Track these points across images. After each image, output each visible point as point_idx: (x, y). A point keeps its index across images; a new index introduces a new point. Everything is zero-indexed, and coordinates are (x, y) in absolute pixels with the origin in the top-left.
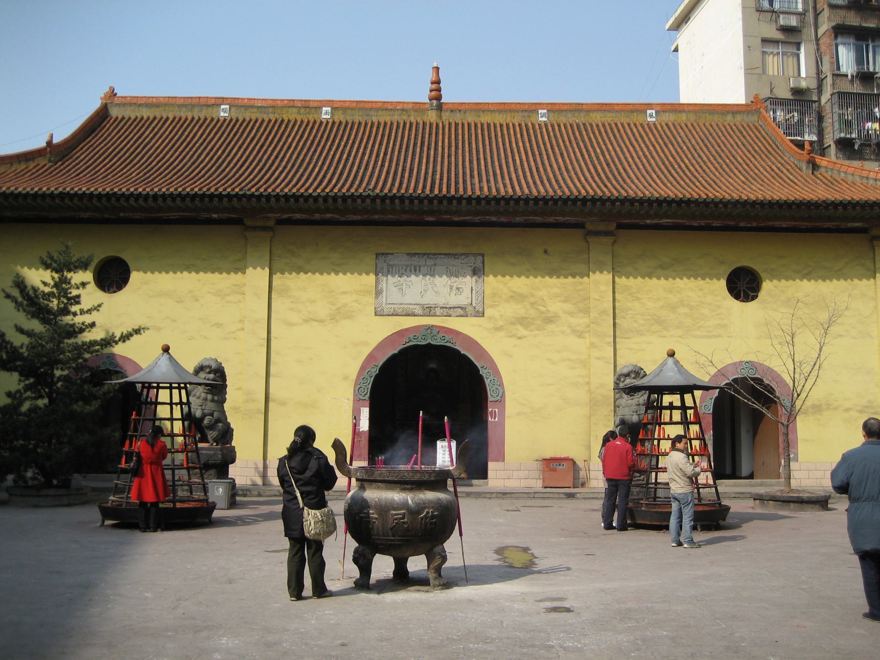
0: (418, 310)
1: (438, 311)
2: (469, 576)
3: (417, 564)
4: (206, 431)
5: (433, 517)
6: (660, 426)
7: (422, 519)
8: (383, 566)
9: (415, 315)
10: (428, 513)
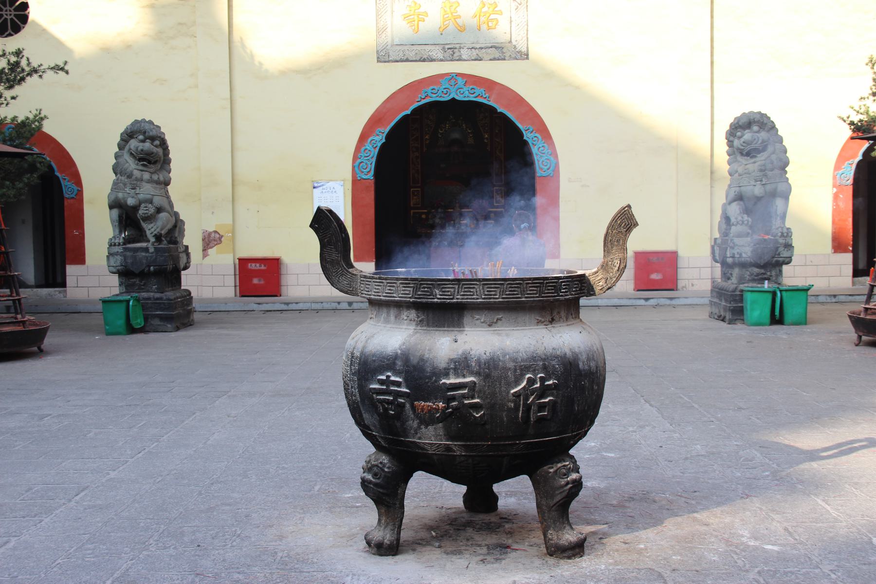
0: (437, 53)
1: (465, 53)
2: (643, 507)
3: (515, 494)
4: (144, 225)
5: (544, 391)
6: (136, 208)
7: (517, 395)
8: (432, 494)
9: (432, 60)
10: (531, 382)
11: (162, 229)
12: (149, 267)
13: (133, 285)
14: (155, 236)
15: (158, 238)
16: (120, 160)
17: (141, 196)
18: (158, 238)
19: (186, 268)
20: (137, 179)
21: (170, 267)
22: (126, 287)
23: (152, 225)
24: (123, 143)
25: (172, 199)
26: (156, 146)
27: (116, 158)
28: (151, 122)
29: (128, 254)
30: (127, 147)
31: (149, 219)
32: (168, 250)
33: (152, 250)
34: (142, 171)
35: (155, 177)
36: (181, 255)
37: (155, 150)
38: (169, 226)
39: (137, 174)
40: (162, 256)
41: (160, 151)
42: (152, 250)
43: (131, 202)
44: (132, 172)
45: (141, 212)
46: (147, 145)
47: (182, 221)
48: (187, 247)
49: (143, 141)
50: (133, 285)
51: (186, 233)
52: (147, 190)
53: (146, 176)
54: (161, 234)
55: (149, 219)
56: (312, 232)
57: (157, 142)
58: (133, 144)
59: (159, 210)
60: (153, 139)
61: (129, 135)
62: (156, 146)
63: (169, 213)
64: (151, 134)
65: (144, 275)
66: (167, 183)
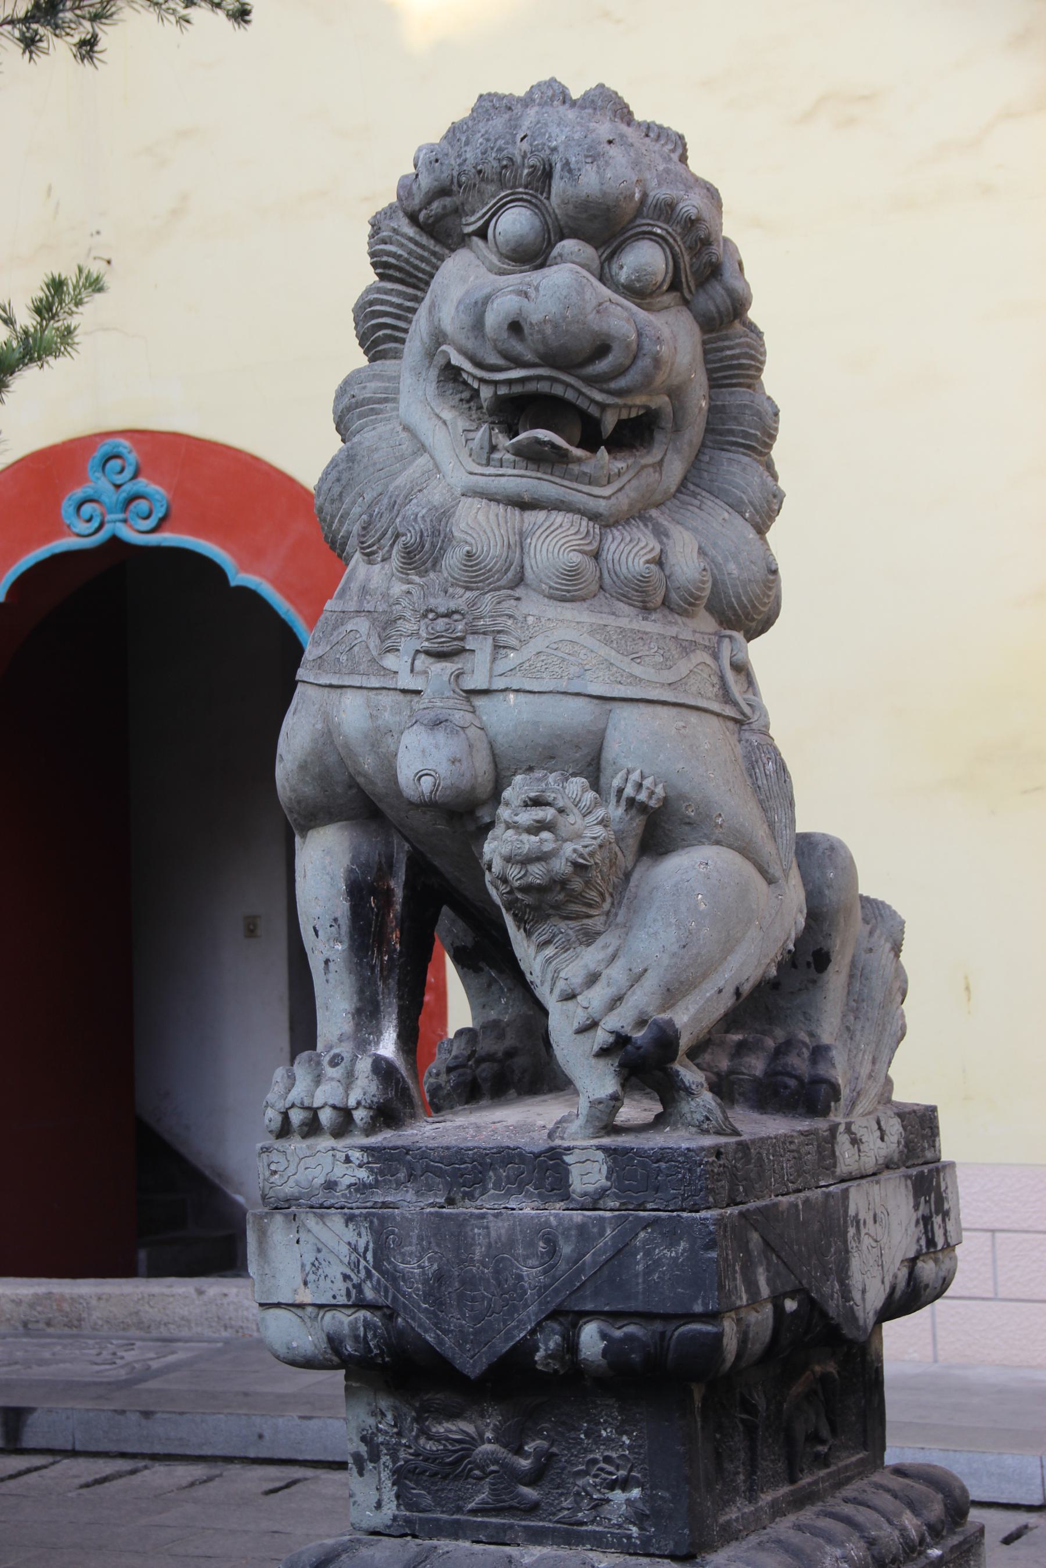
6: (465, 814)
11: (671, 995)
12: (570, 1319)
13: (452, 1468)
14: (619, 1045)
15: (645, 1063)
16: (367, 437)
17: (507, 716)
18: (645, 1063)
19: (910, 1297)
20: (476, 575)
21: (746, 1324)
22: (400, 1476)
23: (591, 957)
24: (395, 293)
25: (782, 733)
26: (639, 293)
27: (342, 425)
28: (608, 103)
29: (410, 1203)
30: (420, 326)
31: (563, 900)
32: (736, 1171)
33: (588, 1174)
34: (524, 505)
35: (630, 552)
36: (860, 1200)
37: (622, 318)
38: (749, 962)
39: (480, 527)
40: (671, 1232)
41: (675, 336)
42: (588, 1174)
43: (423, 763)
44: (444, 515)
45: (494, 848)
46: (564, 288)
47: (876, 912)
48: (922, 1124)
49: (531, 256)
50: (452, 1468)
51: (912, 1009)
52: (556, 661)
53: (554, 543)
54: (665, 1041)
55: (563, 900)
56: (473, 101)
57: (645, 258)
58: (462, 279)
59: (659, 828)
60: (606, 227)
61: (434, 218)
62: (639, 293)
63: (746, 850)
64: (590, 181)
65: (524, 1386)
66: (749, 611)
